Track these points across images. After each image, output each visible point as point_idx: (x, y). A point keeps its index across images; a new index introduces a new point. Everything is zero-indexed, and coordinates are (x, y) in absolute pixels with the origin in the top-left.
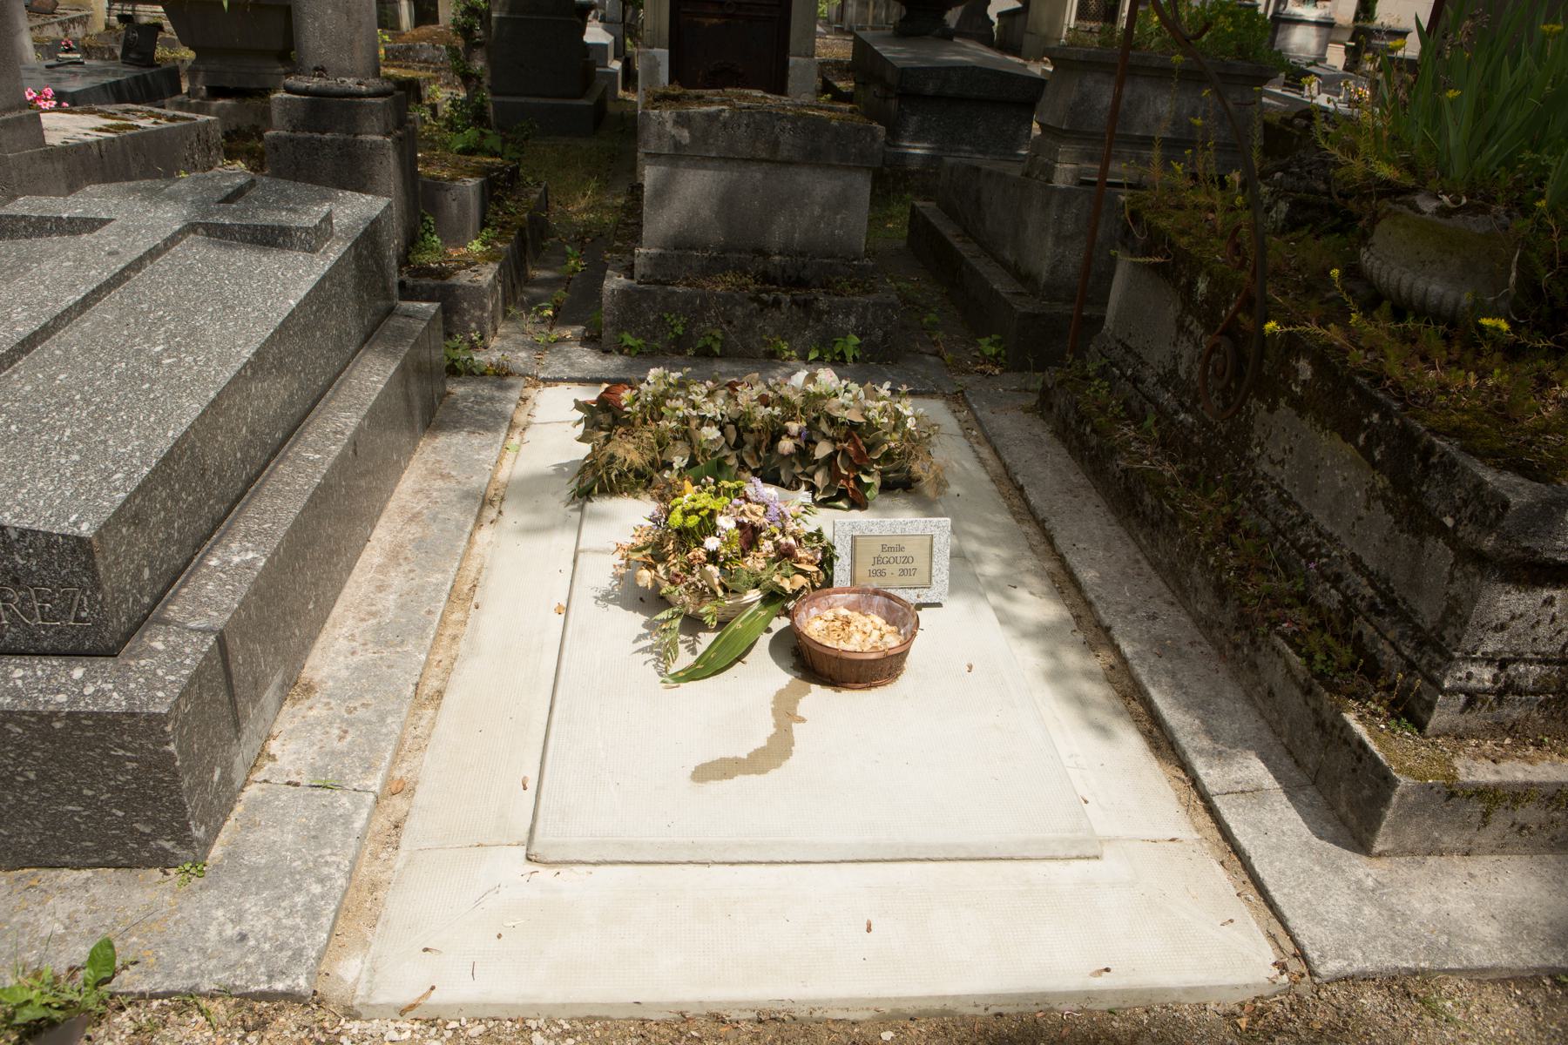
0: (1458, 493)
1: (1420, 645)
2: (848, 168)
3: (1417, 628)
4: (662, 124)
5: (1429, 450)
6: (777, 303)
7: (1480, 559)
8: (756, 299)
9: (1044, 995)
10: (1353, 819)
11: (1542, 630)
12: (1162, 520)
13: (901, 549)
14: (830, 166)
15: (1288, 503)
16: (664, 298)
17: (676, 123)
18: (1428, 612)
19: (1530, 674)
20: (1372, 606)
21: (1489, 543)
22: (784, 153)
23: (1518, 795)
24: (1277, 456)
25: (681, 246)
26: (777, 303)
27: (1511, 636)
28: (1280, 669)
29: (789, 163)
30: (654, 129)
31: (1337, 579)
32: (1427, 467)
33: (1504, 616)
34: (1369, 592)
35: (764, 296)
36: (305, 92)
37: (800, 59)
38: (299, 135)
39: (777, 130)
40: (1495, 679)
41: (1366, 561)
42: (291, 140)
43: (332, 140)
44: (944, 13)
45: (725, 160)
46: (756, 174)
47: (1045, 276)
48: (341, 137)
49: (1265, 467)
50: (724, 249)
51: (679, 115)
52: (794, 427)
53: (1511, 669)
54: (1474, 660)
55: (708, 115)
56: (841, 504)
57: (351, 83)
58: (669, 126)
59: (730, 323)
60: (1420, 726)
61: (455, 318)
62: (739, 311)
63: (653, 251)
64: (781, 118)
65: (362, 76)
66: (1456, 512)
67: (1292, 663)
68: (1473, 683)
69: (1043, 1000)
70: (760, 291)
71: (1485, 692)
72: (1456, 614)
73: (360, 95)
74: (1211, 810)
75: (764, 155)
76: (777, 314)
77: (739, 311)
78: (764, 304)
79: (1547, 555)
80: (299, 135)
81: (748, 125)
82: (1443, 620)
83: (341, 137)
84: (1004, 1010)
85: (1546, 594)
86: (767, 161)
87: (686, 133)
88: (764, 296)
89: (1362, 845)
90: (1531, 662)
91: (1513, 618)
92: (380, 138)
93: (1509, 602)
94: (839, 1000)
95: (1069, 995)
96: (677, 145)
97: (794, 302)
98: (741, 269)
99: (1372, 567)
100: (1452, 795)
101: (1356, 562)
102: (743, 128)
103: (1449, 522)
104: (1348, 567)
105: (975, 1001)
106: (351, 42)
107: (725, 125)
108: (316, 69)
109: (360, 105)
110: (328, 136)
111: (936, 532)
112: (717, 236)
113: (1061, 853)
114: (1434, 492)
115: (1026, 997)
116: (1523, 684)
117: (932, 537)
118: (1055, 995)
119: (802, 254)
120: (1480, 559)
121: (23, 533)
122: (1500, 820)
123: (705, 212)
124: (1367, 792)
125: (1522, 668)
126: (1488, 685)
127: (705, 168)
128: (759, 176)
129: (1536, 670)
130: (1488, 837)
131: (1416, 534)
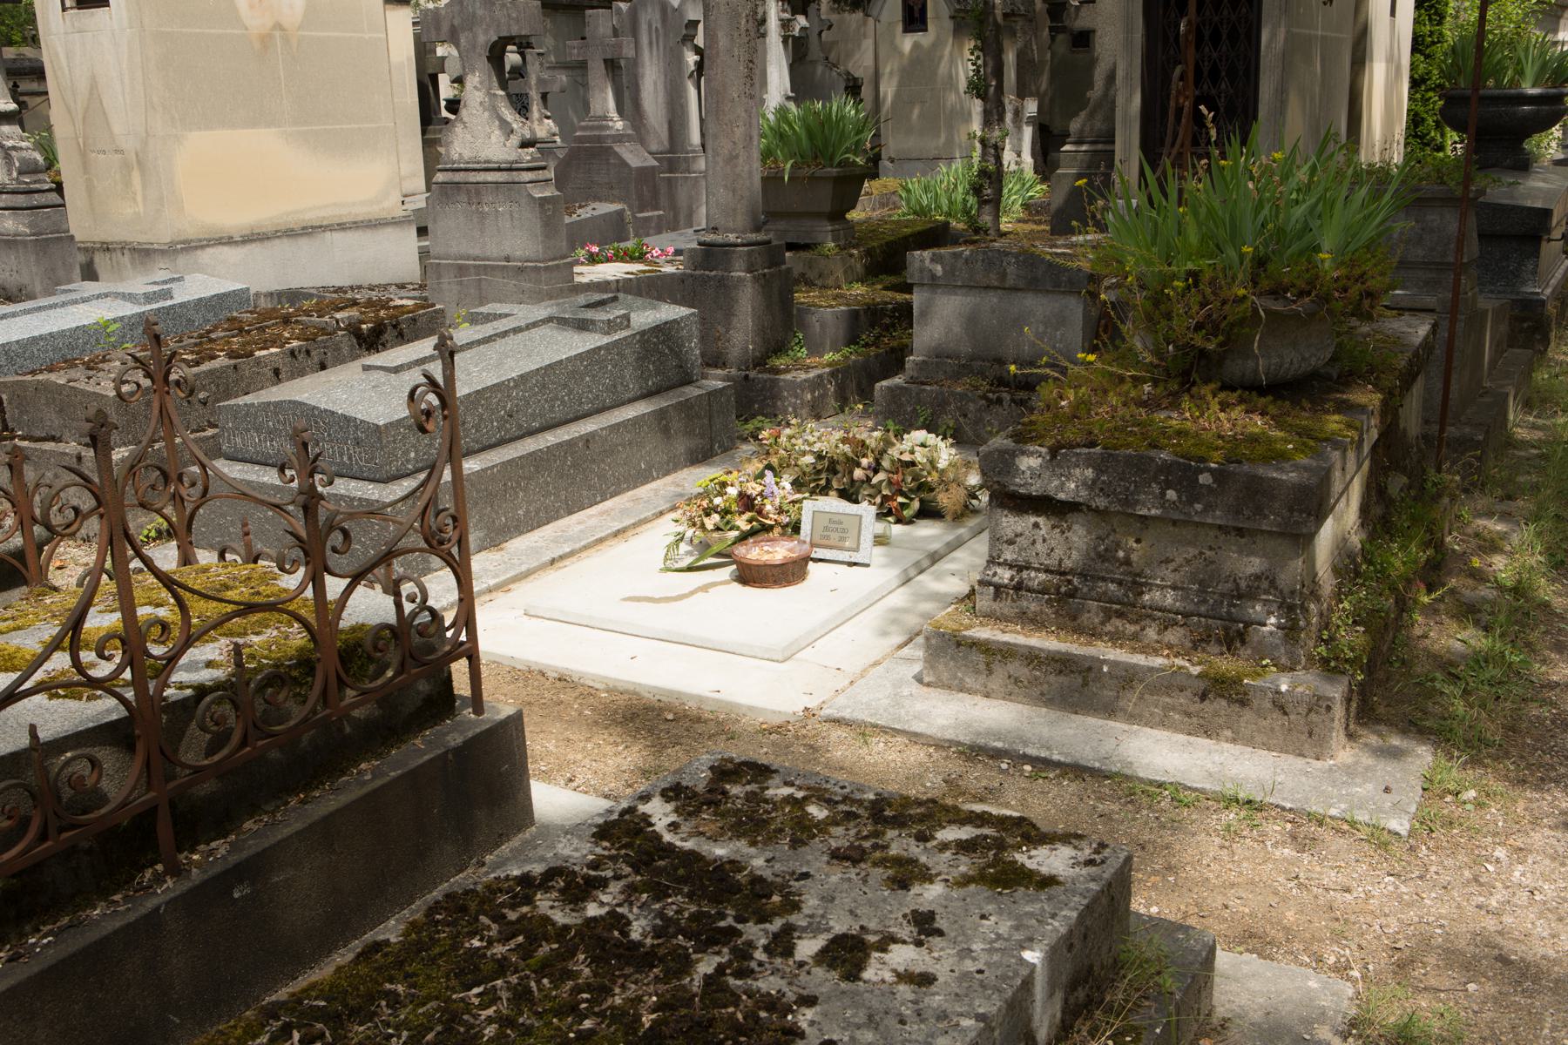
2: (1064, 293)
4: (922, 261)
6: (999, 401)
8: (984, 397)
9: (679, 693)
11: (1039, 546)
13: (841, 523)
16: (917, 394)
17: (932, 260)
19: (1037, 578)
22: (1010, 282)
23: (1007, 653)
25: (940, 354)
26: (999, 401)
27: (1020, 550)
29: (1015, 289)
33: (1011, 535)
35: (990, 395)
38: (697, 272)
39: (1005, 264)
40: (1012, 579)
42: (692, 276)
45: (970, 287)
46: (993, 299)
48: (720, 273)
50: (972, 358)
51: (934, 254)
52: (864, 462)
53: (1025, 574)
54: (999, 564)
55: (954, 254)
56: (890, 519)
57: (732, 238)
58: (927, 262)
59: (965, 416)
61: (779, 403)
62: (972, 407)
63: (920, 358)
64: (1007, 254)
65: (742, 232)
68: (996, 579)
69: (679, 695)
71: (1006, 586)
73: (736, 245)
75: (996, 284)
76: (1000, 410)
77: (972, 407)
78: (990, 401)
79: (1012, 488)
80: (697, 272)
81: (983, 261)
83: (720, 273)
84: (663, 698)
85: (1033, 519)
86: (996, 288)
87: (939, 268)
88: (990, 395)
90: (1038, 570)
91: (1016, 536)
92: (742, 274)
94: (593, 675)
95: (692, 697)
96: (933, 277)
97: (1013, 400)
98: (981, 374)
100: (959, 644)
102: (980, 263)
105: (652, 689)
106: (734, 210)
107: (967, 261)
110: (713, 273)
111: (864, 514)
112: (966, 349)
113: (760, 655)
115: (671, 692)
116: (1030, 584)
117: (861, 517)
118: (685, 694)
121: (361, 421)
122: (1000, 672)
123: (957, 329)
125: (1033, 574)
126: (1006, 581)
127: (956, 294)
129: (1042, 576)
130: (996, 682)
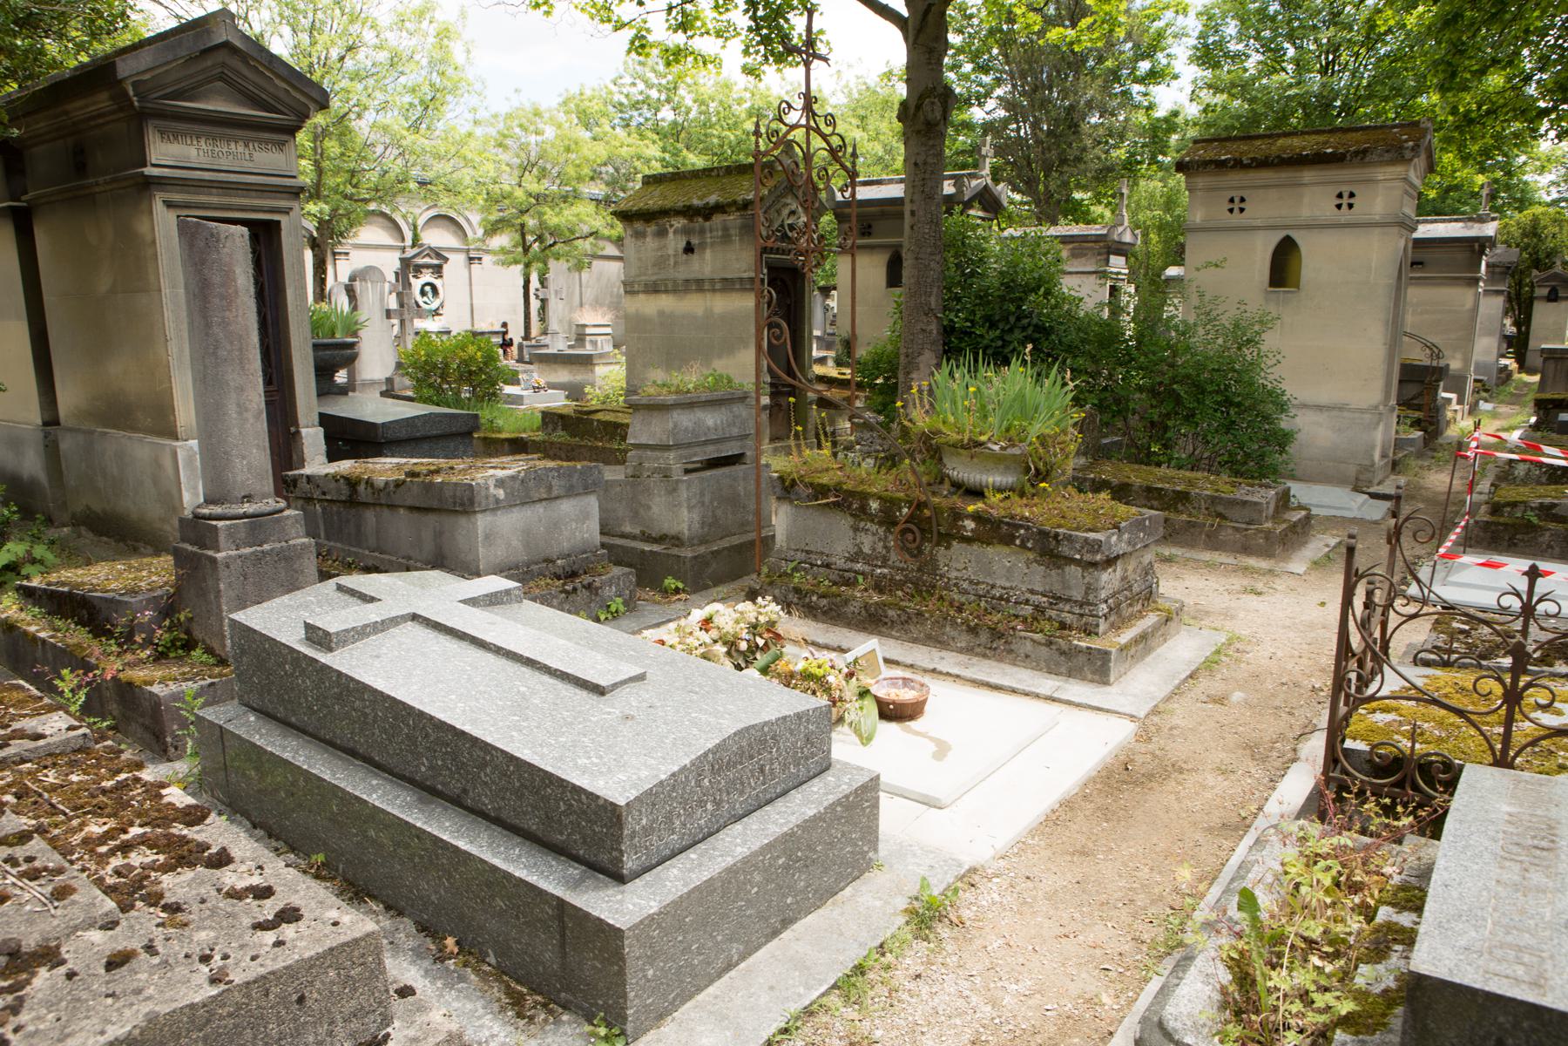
0: (1078, 546)
1: (1081, 606)
3: (1076, 602)
5: (1057, 535)
7: (1094, 565)
10: (1096, 677)
12: (909, 618)
14: (579, 494)
15: (978, 583)
18: (1077, 595)
20: (1051, 604)
21: (1098, 557)
22: (555, 493)
24: (961, 566)
28: (1028, 644)
30: (483, 493)
31: (1027, 602)
32: (1058, 542)
34: (1045, 599)
36: (245, 516)
37: (310, 430)
41: (1036, 588)
43: (272, 550)
44: (333, 376)
47: (686, 532)
48: (278, 545)
49: (953, 574)
60: (1097, 634)
66: (1079, 552)
67: (1294, 513)
70: (564, 584)
72: (1089, 589)
74: (1054, 700)
82: (1086, 593)
83: (278, 545)
89: (1106, 683)
93: (1105, 576)
96: (497, 501)
99: (1041, 589)
101: (1032, 592)
103: (1078, 557)
104: (1028, 596)
108: (244, 497)
109: (278, 521)
110: (266, 547)
114: (1066, 549)
119: (569, 555)
120: (1094, 565)
124: (1099, 663)
128: (541, 510)
131: (1059, 568)
